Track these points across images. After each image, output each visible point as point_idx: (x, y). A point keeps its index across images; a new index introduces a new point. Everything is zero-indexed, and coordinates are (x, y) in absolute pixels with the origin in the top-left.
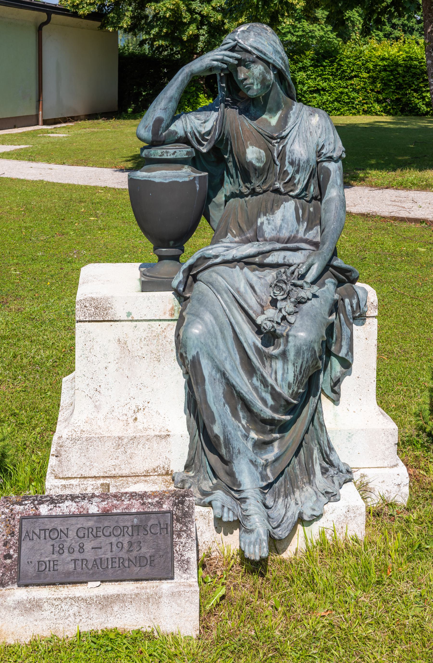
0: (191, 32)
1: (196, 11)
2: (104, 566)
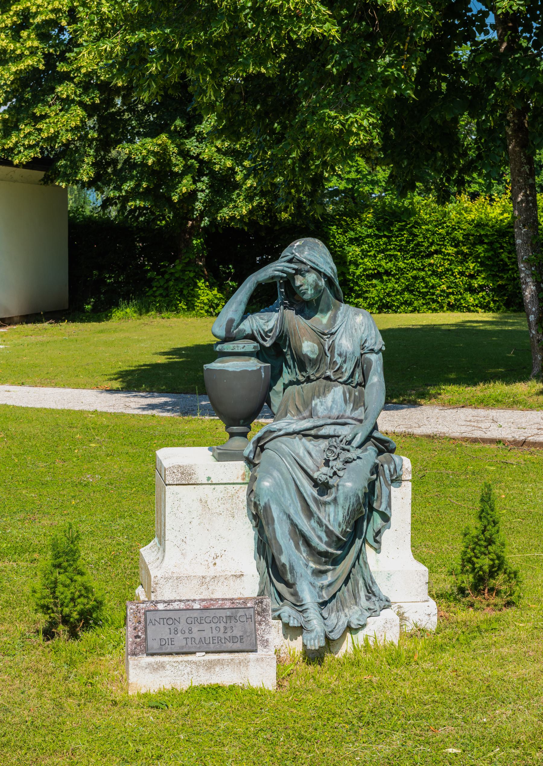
0: (184, 190)
1: (192, 153)
2: (207, 642)
